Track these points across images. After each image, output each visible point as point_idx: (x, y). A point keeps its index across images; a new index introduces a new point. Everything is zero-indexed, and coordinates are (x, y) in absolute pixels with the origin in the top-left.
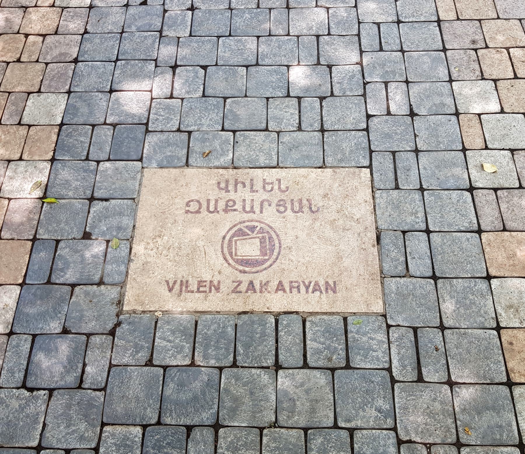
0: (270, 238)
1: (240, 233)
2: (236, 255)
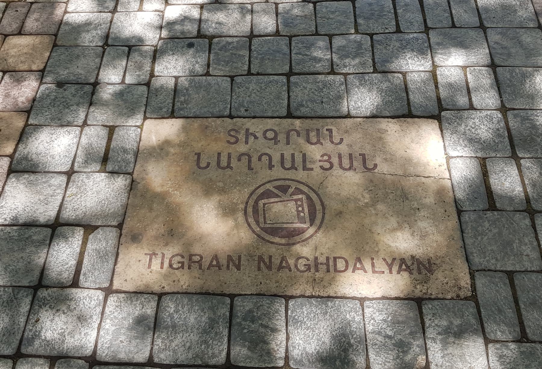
0: (309, 198)
1: (262, 196)
2: (265, 223)
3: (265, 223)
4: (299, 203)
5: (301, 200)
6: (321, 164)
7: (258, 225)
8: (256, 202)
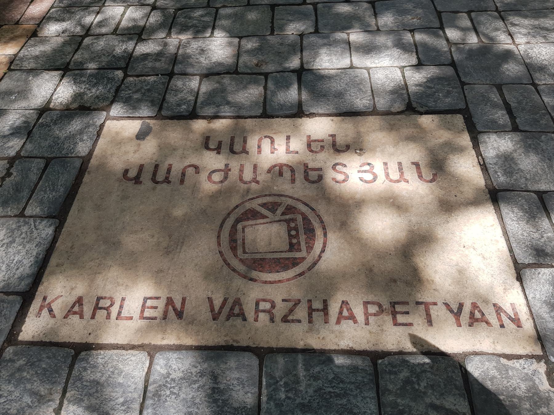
2: (244, 252)
3: (244, 252)
4: (292, 225)
5: (293, 220)
6: (361, 175)
7: (236, 256)
8: (234, 227)
